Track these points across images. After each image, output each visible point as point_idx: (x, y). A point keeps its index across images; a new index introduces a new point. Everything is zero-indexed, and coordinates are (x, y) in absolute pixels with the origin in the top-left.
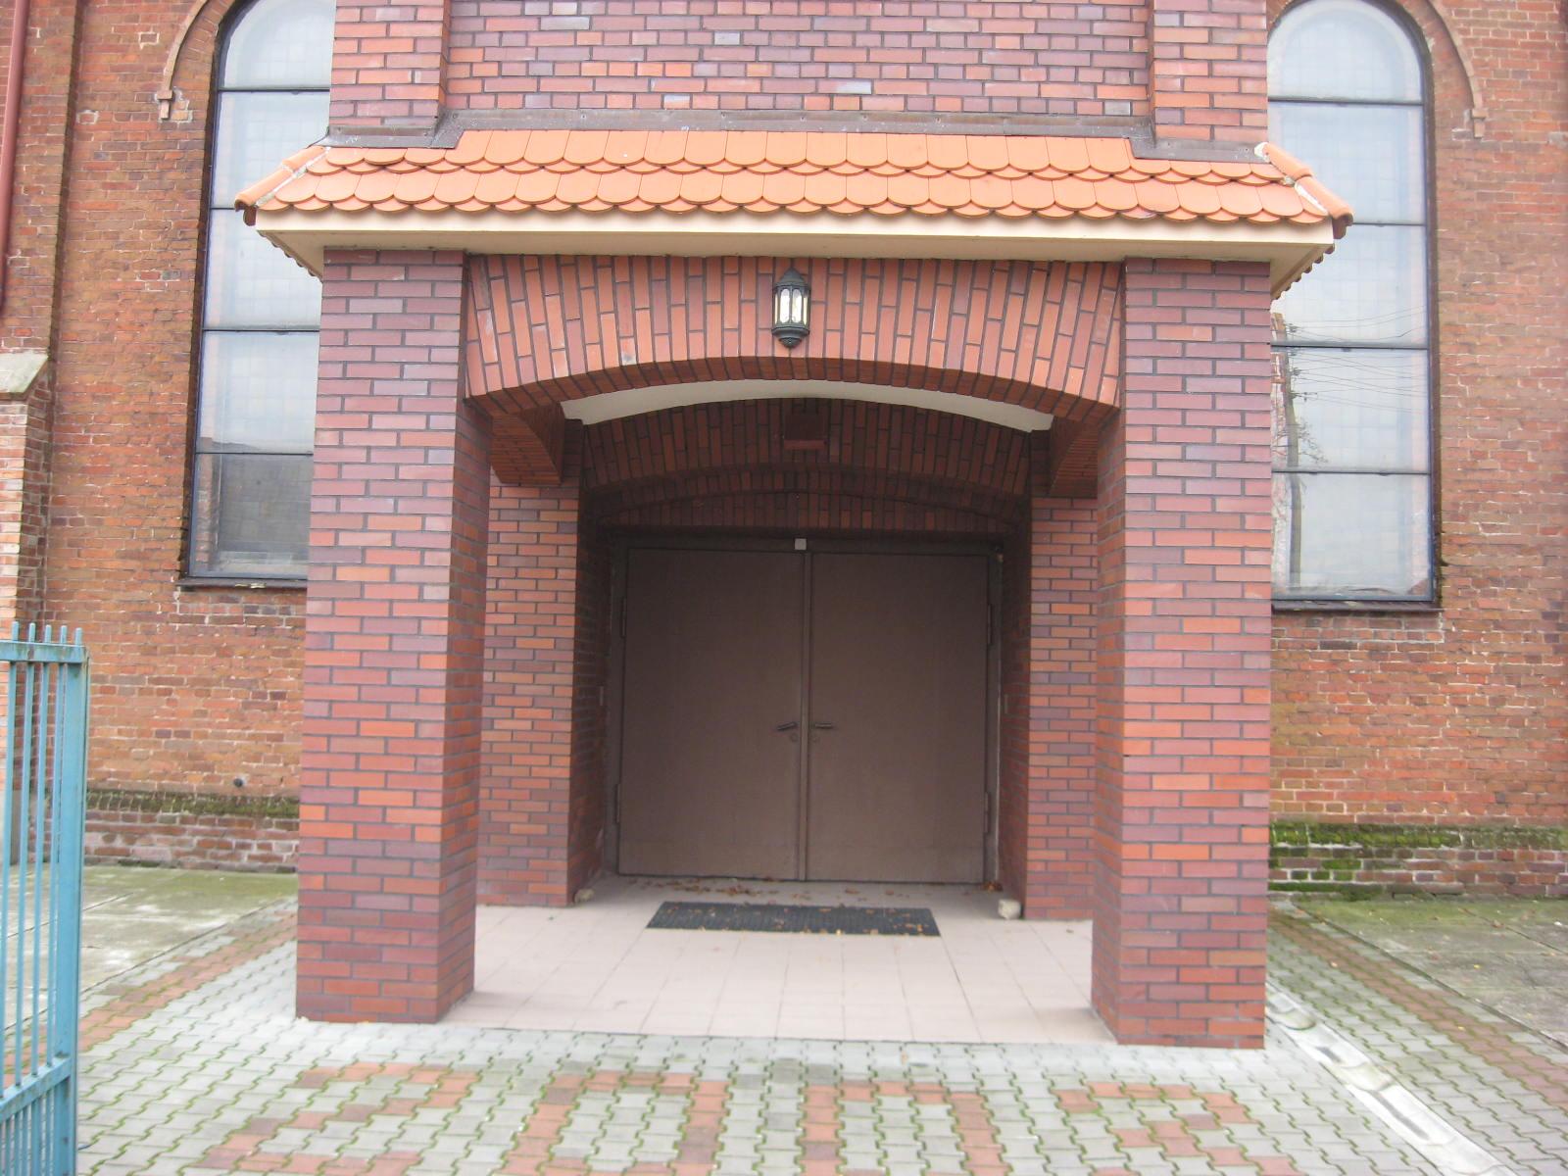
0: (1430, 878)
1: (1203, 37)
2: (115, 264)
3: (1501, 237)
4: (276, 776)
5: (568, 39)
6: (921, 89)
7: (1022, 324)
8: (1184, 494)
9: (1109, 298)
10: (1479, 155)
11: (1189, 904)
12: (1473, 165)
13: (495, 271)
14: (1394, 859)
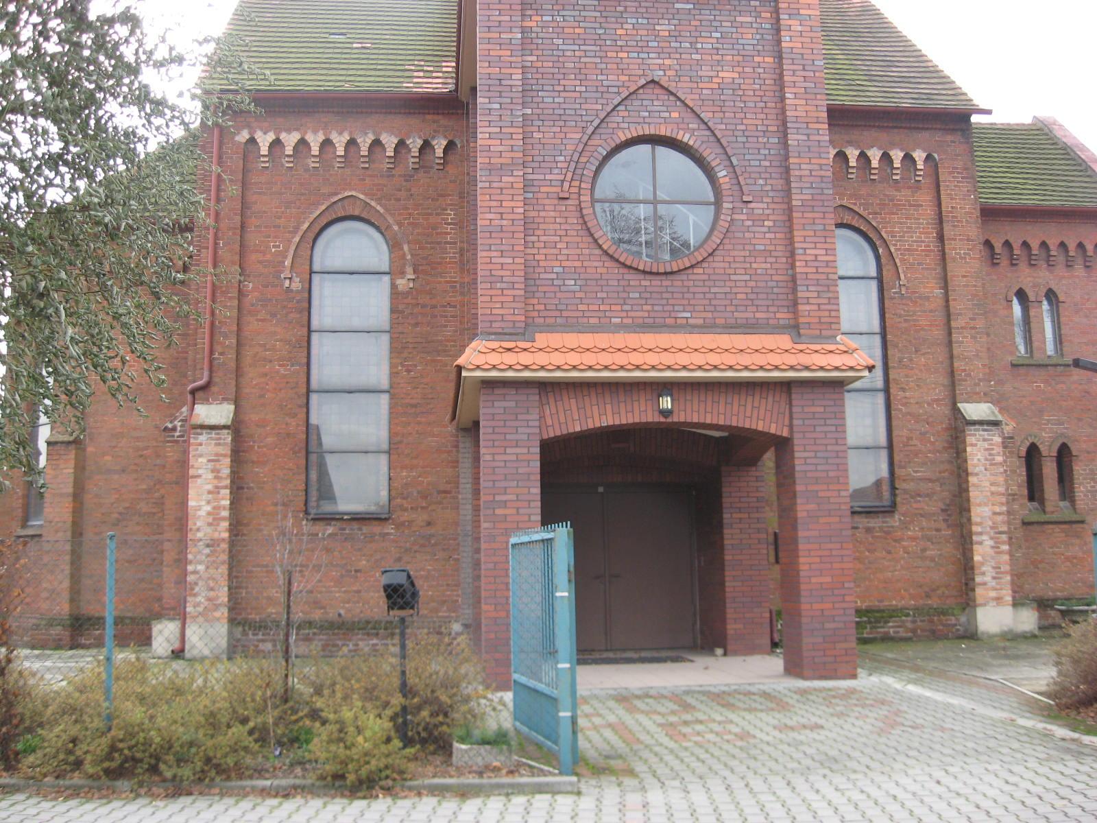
0: (898, 632)
1: (815, 295)
2: (265, 359)
3: (915, 339)
4: (358, 610)
5: (571, 295)
6: (710, 315)
7: (753, 407)
8: (816, 470)
9: (784, 396)
10: (904, 302)
11: (827, 626)
12: (901, 307)
13: (549, 389)
14: (882, 624)
